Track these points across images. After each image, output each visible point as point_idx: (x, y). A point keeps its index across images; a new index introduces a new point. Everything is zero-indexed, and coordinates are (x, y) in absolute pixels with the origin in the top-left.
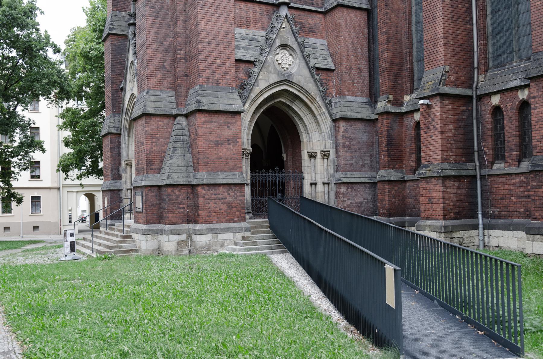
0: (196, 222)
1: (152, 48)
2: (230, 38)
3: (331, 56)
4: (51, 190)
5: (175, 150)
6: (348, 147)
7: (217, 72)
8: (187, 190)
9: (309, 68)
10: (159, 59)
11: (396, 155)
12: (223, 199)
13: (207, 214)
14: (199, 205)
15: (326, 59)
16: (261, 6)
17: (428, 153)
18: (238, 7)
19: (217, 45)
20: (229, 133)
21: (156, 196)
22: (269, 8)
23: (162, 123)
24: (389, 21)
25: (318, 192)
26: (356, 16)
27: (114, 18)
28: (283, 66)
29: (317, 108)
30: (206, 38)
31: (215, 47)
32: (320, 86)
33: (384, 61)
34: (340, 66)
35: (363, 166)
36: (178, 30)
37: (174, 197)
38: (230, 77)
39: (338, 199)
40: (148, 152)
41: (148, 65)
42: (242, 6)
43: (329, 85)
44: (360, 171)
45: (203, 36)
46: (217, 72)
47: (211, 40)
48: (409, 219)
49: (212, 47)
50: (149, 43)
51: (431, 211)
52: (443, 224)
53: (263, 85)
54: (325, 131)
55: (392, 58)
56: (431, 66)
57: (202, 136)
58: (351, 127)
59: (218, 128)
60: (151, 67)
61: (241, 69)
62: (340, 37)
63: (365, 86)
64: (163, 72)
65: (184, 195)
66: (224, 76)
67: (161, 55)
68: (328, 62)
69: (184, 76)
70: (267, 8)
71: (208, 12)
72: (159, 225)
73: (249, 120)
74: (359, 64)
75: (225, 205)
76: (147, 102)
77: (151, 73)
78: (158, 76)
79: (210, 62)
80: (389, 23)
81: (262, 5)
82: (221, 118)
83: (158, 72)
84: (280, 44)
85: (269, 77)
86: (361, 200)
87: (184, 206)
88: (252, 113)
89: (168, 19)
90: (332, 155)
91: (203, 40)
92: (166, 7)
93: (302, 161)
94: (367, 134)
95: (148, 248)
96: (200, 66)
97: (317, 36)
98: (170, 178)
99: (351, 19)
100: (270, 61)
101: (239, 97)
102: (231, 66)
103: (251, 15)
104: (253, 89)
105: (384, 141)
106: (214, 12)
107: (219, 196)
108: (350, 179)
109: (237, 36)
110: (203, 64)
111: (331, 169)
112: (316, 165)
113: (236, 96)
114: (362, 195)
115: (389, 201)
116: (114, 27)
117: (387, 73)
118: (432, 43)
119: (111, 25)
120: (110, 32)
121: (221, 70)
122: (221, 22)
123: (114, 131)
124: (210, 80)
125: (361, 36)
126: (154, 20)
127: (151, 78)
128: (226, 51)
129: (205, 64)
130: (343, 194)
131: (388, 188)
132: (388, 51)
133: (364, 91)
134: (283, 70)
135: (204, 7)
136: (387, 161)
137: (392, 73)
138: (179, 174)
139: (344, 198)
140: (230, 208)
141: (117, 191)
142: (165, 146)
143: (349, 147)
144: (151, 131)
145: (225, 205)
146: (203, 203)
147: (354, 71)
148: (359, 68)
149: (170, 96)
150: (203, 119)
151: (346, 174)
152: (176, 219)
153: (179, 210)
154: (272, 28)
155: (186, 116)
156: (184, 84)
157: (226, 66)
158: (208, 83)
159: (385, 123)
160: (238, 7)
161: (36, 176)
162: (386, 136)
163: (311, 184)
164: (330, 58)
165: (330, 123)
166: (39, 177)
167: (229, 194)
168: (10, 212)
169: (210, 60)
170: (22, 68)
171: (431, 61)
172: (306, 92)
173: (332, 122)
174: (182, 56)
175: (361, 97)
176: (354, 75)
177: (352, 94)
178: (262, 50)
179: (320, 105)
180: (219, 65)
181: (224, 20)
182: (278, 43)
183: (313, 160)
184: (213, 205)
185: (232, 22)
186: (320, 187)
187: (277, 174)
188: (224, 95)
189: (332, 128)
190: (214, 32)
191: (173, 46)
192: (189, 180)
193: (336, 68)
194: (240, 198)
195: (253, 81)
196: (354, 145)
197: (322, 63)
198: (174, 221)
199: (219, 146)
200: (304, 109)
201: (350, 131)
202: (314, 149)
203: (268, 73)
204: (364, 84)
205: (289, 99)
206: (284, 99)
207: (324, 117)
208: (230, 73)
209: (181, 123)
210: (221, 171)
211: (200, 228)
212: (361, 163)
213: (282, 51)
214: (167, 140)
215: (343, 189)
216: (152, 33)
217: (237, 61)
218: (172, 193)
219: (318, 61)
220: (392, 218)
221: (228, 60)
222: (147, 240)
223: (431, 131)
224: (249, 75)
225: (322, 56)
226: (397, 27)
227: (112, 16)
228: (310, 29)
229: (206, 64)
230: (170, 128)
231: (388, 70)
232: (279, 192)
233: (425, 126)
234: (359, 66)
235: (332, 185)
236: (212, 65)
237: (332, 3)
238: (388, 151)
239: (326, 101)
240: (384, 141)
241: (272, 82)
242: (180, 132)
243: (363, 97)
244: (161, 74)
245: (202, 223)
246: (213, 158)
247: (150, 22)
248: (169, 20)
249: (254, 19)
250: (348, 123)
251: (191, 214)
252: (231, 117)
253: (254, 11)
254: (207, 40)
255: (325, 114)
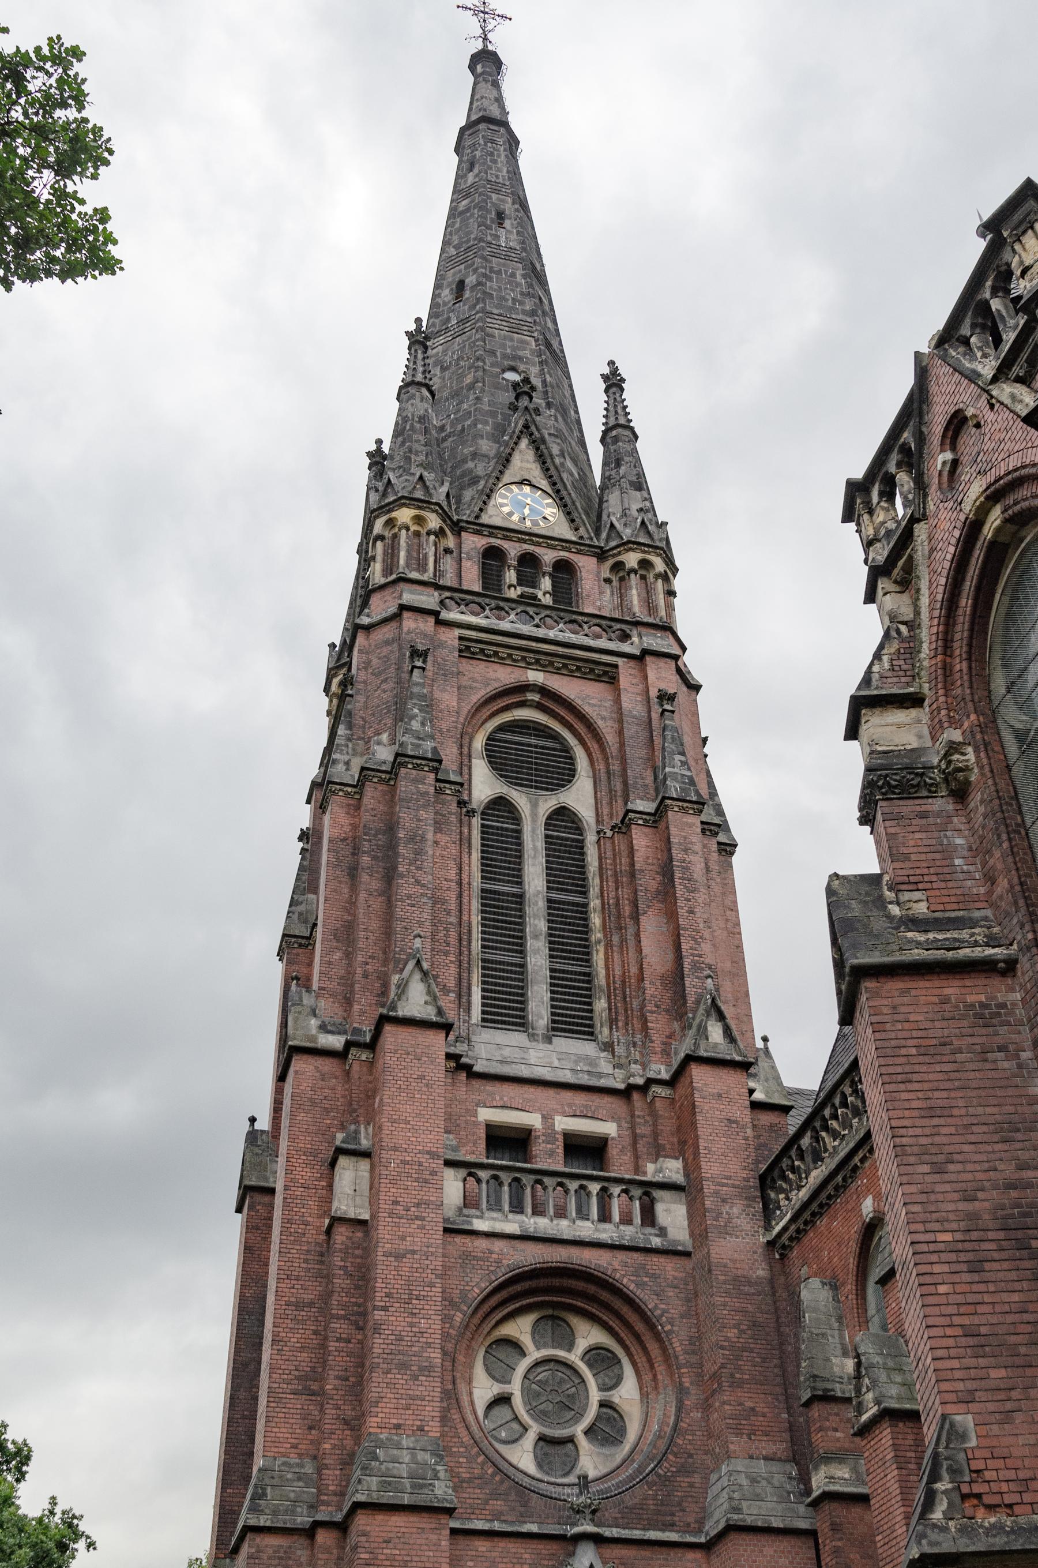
18: (474, 1553)
26: (783, 1552)
42: (484, 1549)
70: (548, 1547)
81: (535, 1541)
160: (474, 1553)
170: (405, 439)
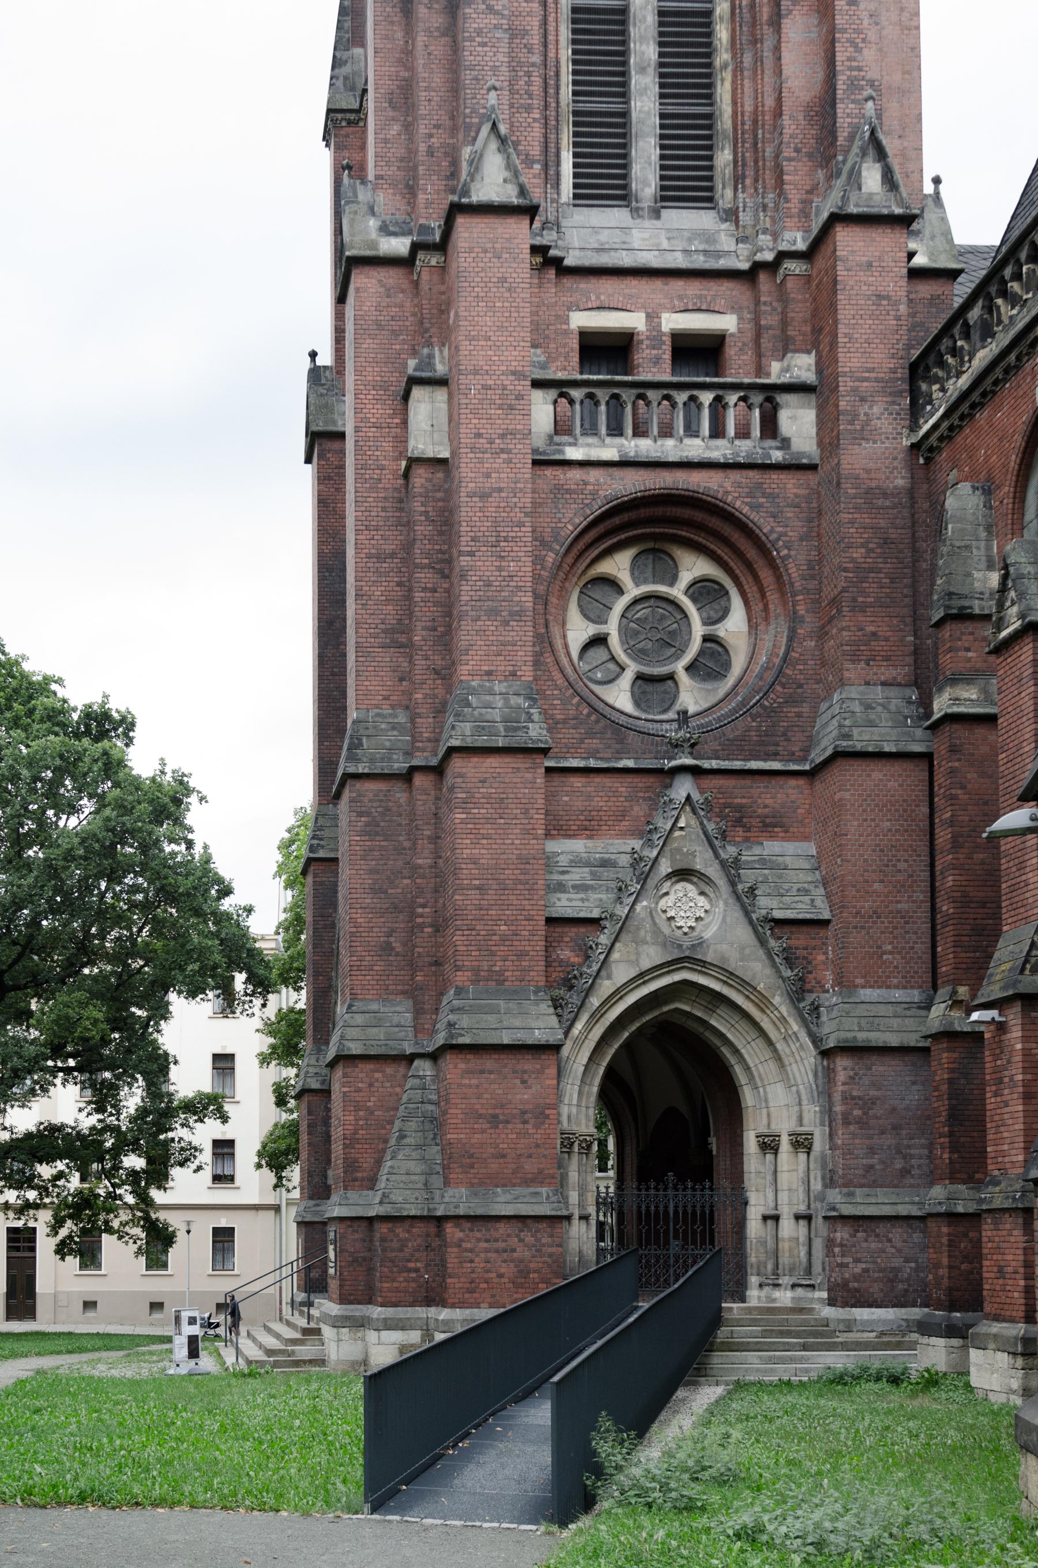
0: (443, 1303)
1: (363, 905)
2: (532, 872)
3: (824, 884)
4: (260, 1212)
5: (404, 1137)
6: (858, 1123)
7: (499, 953)
8: (425, 1230)
9: (751, 922)
10: (378, 930)
11: (977, 1145)
12: (505, 1251)
13: (468, 1285)
14: (448, 1265)
15: (806, 892)
16: (629, 779)
17: (999, 1148)
19: (501, 892)
20: (524, 1096)
21: (365, 1241)
22: (652, 780)
23: (380, 1075)
24: (959, 792)
25: (783, 1240)
26: (893, 776)
27: (320, 822)
28: (679, 925)
29: (778, 1022)
30: (473, 877)
31: (494, 897)
32: (782, 968)
33: (945, 897)
34: (841, 912)
35: (905, 1172)
36: (420, 861)
37: (395, 1244)
38: (532, 963)
39: (832, 1259)
40: (348, 1142)
41: (353, 944)
42: (579, 785)
43: (814, 962)
44: (896, 1186)
45: (467, 872)
46: (499, 953)
47: (485, 882)
48: (962, 1318)
49: (489, 897)
50: (355, 896)
51: (1003, 1299)
52: (1022, 1332)
53: (621, 973)
54: (799, 1081)
55: (968, 889)
56: (1015, 919)
57: (459, 1106)
58: (870, 1069)
59: (497, 1086)
60: (359, 949)
61: (567, 939)
62: (841, 835)
63: (920, 958)
64: (385, 958)
65: (419, 1241)
66: (516, 963)
67: (382, 920)
68: (813, 901)
69: (431, 964)
71: (481, 816)
72: (370, 1306)
73: (585, 1061)
74: (898, 902)
75: (512, 1265)
76: (348, 1029)
77: (359, 963)
78: (375, 968)
79: (482, 933)
80: (960, 797)
81: (631, 776)
82: (506, 1061)
83: (375, 958)
84: (670, 870)
85: (638, 954)
86: (897, 1262)
87: (419, 1265)
88: (592, 1045)
89: (400, 835)
90: (819, 1145)
91: (465, 882)
92: (395, 809)
93: (745, 1158)
94: (921, 1088)
95: (342, 1357)
96: (458, 943)
97: (788, 835)
98: (387, 1201)
99: (875, 785)
100: (643, 915)
101: (552, 1010)
102: (536, 938)
103: (601, 804)
104: (597, 986)
105: (942, 1108)
106: (495, 816)
107: (496, 1245)
108: (862, 1207)
109: (563, 860)
110: (465, 938)
111: (815, 1179)
112: (779, 1169)
113: (546, 1008)
114: (899, 1251)
115: (950, 1267)
116: (322, 843)
117: (951, 928)
118: (1017, 861)
119: (313, 838)
120: (312, 855)
121: (510, 948)
122: (510, 836)
123: (315, 1085)
124: (482, 973)
125: (909, 825)
126: (367, 843)
127: (358, 973)
128: (524, 902)
129: (470, 938)
130: (841, 1245)
131: (949, 1235)
132: (955, 872)
133: (916, 972)
134: (679, 933)
135: (469, 805)
136: (947, 1161)
137: (969, 927)
138: (408, 1192)
139: (843, 1256)
140: (524, 1273)
141: (320, 1226)
142: (388, 1127)
143: (862, 1123)
144: (356, 1094)
145: (512, 1265)
146: (456, 1260)
147: (883, 922)
148: (898, 912)
149: (401, 1013)
150: (462, 1066)
151: (851, 1194)
152: (399, 1295)
153: (405, 1274)
154: (650, 832)
155: (434, 1056)
156: (431, 983)
157: (522, 938)
158: (475, 982)
159: (944, 1057)
161: (226, 1177)
162: (946, 1097)
163: (765, 1218)
164: (821, 891)
165: (813, 1060)
166: (231, 1179)
167: (521, 1240)
168: (99, 1267)
169: (482, 927)
171: (1014, 906)
172: (744, 985)
173: (819, 1057)
174: (426, 920)
175: (905, 987)
176: (882, 933)
177: (875, 982)
178: (620, 889)
179: (785, 1014)
180: (504, 938)
181: (518, 831)
182: (665, 867)
183: (769, 1157)
184: (482, 1265)
185: (540, 832)
186: (788, 1227)
187: (670, 1192)
188: (515, 1007)
189: (820, 1074)
190: (494, 861)
191: (409, 896)
192: (431, 1206)
193: (833, 916)
194: (550, 1250)
195: (595, 967)
196: (877, 1118)
197: (794, 905)
198: (394, 1299)
199: (501, 1126)
200: (743, 1025)
201: (866, 1081)
202: (773, 1126)
203: (637, 943)
204: (916, 953)
205: (703, 1002)
206: (684, 1003)
207: (798, 1044)
208: (531, 953)
209: (421, 1073)
210: (504, 1186)
211: (448, 1317)
212: (899, 1164)
213: (680, 886)
214: (392, 1113)
215: (841, 1234)
216: (362, 872)
217: (550, 921)
218: (391, 1234)
219: (781, 902)
220: (958, 1315)
221: (527, 923)
222: (339, 1340)
223: (1006, 1091)
224: (586, 952)
225: (796, 887)
226: (986, 803)
227: (317, 818)
228: (768, 820)
229: (472, 938)
230: (400, 1086)
231: (955, 921)
232: (676, 1237)
233: (994, 1076)
234: (899, 906)
235: (818, 1222)
236: (487, 938)
237: (825, 749)
238: (951, 1134)
239: (801, 1005)
240: (942, 1108)
241: (646, 964)
242: (417, 1095)
243: (912, 987)
244: (383, 963)
245: (453, 1306)
246: (484, 1156)
247: (358, 848)
248: (401, 838)
249: (608, 813)
250: (861, 1058)
251: (434, 1285)
252: (530, 1057)
253: (611, 794)
254: (477, 882)
255: (798, 1039)
